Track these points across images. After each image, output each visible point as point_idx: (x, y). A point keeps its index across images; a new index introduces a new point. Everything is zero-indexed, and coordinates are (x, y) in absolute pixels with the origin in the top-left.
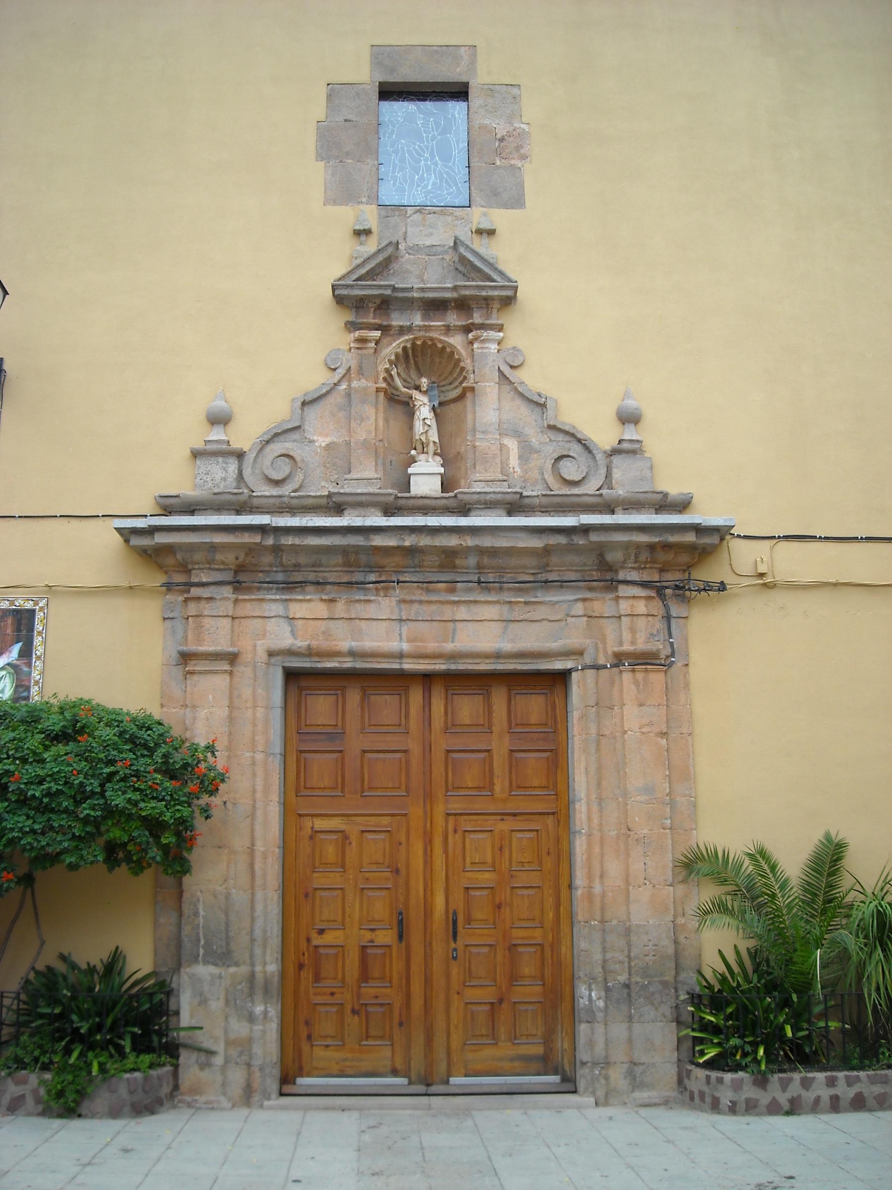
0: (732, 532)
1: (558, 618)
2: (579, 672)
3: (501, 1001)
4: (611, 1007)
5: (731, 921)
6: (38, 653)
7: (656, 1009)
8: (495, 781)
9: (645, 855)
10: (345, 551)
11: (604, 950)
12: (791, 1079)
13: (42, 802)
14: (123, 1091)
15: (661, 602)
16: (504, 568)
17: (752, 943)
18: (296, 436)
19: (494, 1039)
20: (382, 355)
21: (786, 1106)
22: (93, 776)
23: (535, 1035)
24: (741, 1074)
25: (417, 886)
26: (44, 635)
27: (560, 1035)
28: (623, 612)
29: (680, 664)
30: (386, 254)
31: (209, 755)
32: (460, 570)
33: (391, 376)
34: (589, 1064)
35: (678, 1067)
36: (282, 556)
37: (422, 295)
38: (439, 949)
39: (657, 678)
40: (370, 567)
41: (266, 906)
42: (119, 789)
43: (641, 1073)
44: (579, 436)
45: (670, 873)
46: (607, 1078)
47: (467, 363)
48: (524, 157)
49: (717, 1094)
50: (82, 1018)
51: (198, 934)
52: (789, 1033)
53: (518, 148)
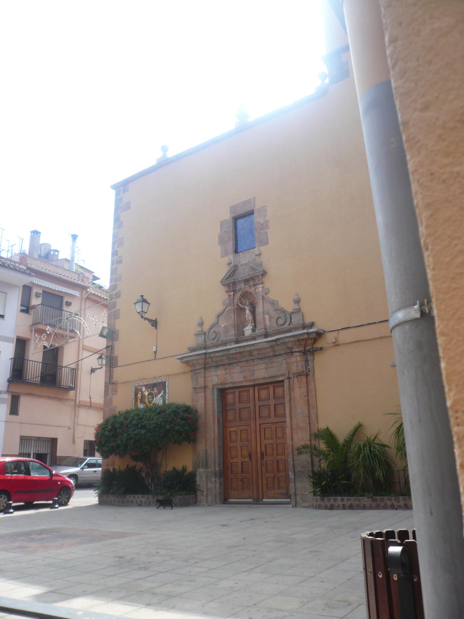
2: (286, 380)
10: (226, 355)
11: (293, 461)
12: (330, 499)
18: (217, 325)
21: (329, 507)
38: (259, 461)
48: (268, 228)
53: (267, 225)
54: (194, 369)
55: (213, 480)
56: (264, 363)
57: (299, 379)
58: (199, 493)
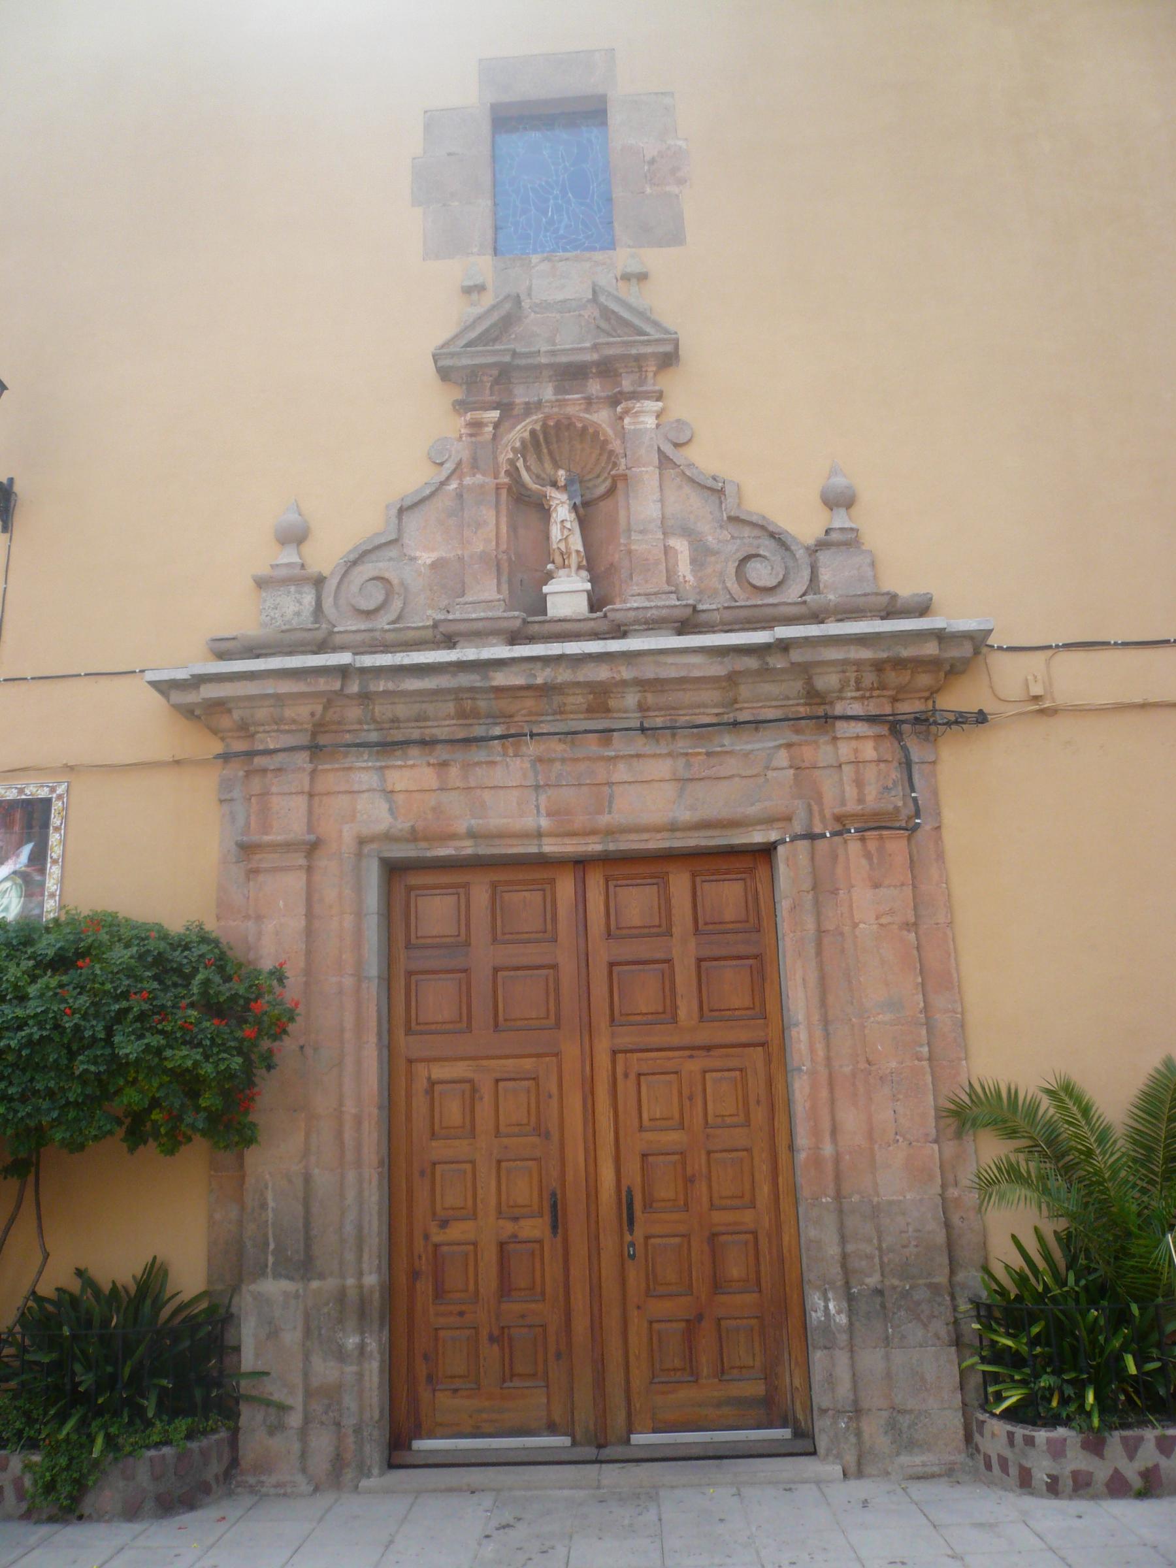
0: (989, 642)
1: (755, 772)
2: (787, 845)
3: (700, 1317)
4: (857, 1324)
5: (1029, 1194)
6: (55, 856)
7: (925, 1326)
8: (679, 1003)
9: (895, 1099)
10: (456, 693)
11: (843, 1240)
12: (1141, 1439)
13: (20, 1056)
14: (143, 1476)
15: (896, 744)
16: (673, 708)
17: (1062, 1224)
18: (393, 552)
19: (692, 1374)
20: (503, 442)
21: (1137, 1483)
22: (96, 1016)
23: (753, 1367)
24: (1061, 1431)
25: (576, 1155)
26: (63, 832)
27: (787, 1364)
28: (843, 759)
29: (928, 828)
30: (502, 312)
31: (275, 982)
32: (615, 715)
33: (517, 469)
34: (830, 1412)
35: (964, 1415)
36: (374, 708)
37: (553, 360)
38: (608, 1242)
39: (896, 846)
40: (493, 717)
41: (361, 1191)
42: (133, 1032)
43: (909, 1427)
44: (771, 528)
45: (932, 1122)
46: (858, 1434)
47: (616, 445)
48: (681, 182)
49: (1028, 1465)
50: (88, 1368)
51: (266, 1236)
52: (1132, 1370)
54: (239, 746)
55: (352, 1342)
56: (670, 755)
57: (872, 845)
58: (250, 1417)
